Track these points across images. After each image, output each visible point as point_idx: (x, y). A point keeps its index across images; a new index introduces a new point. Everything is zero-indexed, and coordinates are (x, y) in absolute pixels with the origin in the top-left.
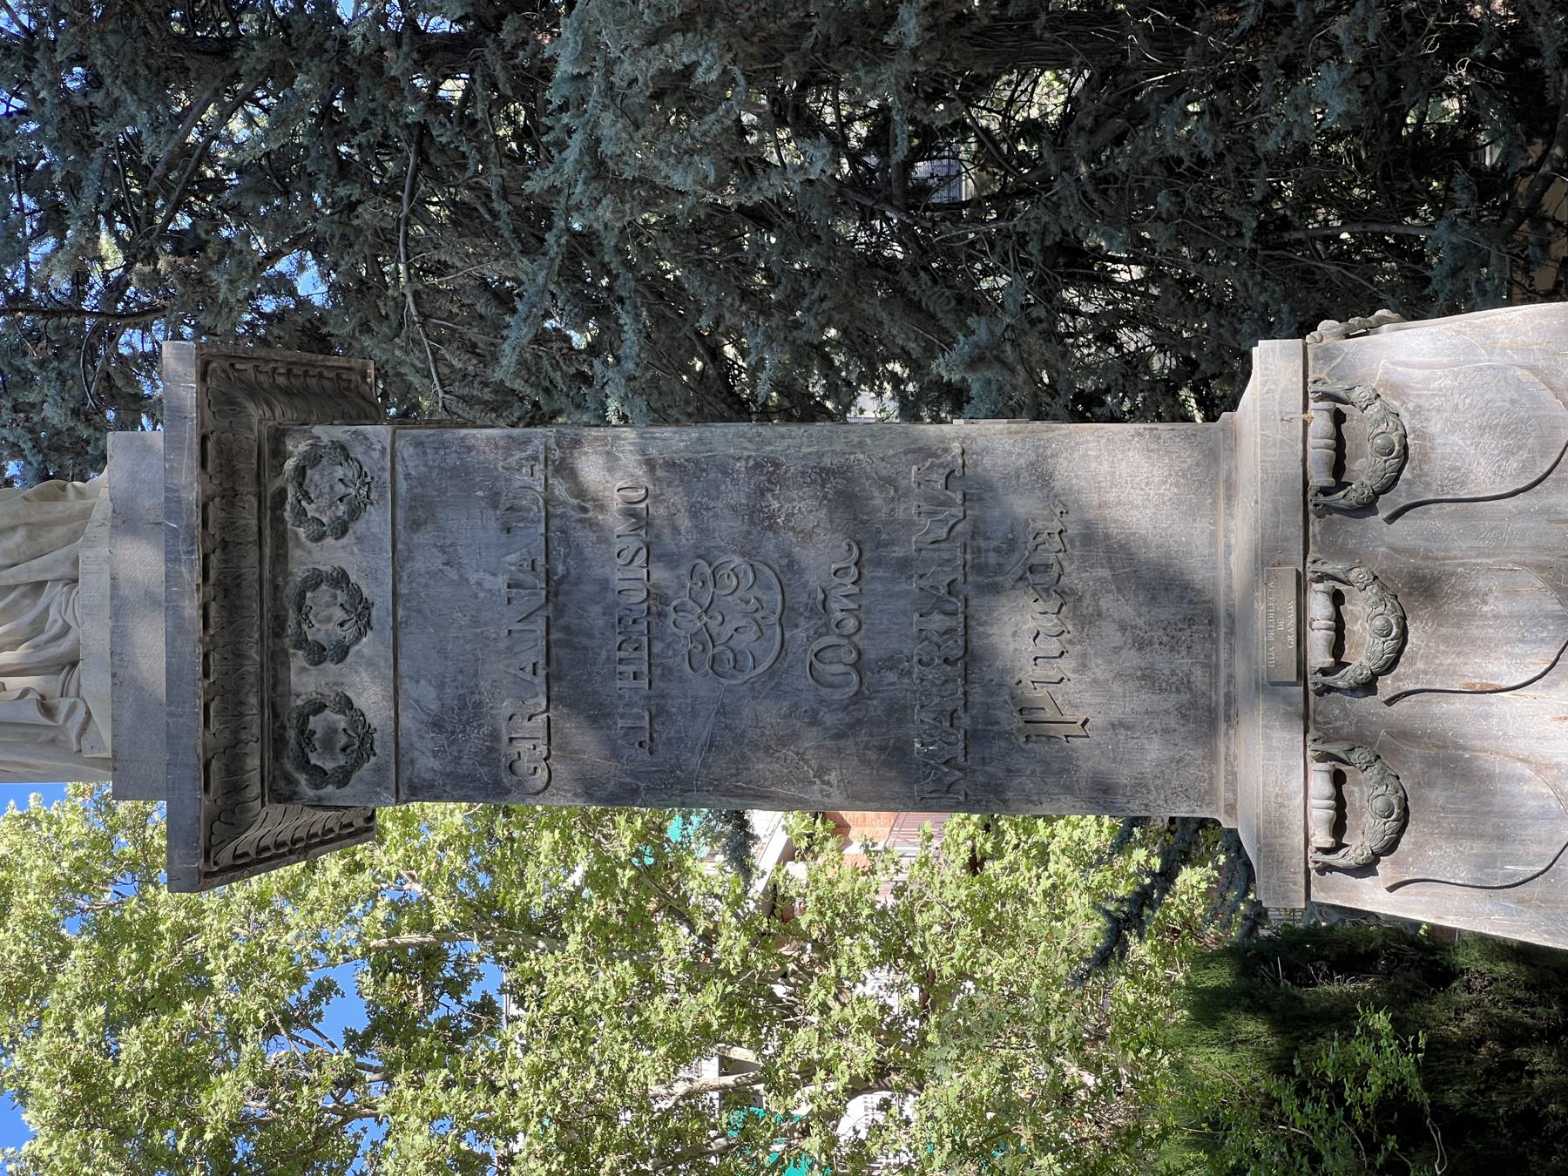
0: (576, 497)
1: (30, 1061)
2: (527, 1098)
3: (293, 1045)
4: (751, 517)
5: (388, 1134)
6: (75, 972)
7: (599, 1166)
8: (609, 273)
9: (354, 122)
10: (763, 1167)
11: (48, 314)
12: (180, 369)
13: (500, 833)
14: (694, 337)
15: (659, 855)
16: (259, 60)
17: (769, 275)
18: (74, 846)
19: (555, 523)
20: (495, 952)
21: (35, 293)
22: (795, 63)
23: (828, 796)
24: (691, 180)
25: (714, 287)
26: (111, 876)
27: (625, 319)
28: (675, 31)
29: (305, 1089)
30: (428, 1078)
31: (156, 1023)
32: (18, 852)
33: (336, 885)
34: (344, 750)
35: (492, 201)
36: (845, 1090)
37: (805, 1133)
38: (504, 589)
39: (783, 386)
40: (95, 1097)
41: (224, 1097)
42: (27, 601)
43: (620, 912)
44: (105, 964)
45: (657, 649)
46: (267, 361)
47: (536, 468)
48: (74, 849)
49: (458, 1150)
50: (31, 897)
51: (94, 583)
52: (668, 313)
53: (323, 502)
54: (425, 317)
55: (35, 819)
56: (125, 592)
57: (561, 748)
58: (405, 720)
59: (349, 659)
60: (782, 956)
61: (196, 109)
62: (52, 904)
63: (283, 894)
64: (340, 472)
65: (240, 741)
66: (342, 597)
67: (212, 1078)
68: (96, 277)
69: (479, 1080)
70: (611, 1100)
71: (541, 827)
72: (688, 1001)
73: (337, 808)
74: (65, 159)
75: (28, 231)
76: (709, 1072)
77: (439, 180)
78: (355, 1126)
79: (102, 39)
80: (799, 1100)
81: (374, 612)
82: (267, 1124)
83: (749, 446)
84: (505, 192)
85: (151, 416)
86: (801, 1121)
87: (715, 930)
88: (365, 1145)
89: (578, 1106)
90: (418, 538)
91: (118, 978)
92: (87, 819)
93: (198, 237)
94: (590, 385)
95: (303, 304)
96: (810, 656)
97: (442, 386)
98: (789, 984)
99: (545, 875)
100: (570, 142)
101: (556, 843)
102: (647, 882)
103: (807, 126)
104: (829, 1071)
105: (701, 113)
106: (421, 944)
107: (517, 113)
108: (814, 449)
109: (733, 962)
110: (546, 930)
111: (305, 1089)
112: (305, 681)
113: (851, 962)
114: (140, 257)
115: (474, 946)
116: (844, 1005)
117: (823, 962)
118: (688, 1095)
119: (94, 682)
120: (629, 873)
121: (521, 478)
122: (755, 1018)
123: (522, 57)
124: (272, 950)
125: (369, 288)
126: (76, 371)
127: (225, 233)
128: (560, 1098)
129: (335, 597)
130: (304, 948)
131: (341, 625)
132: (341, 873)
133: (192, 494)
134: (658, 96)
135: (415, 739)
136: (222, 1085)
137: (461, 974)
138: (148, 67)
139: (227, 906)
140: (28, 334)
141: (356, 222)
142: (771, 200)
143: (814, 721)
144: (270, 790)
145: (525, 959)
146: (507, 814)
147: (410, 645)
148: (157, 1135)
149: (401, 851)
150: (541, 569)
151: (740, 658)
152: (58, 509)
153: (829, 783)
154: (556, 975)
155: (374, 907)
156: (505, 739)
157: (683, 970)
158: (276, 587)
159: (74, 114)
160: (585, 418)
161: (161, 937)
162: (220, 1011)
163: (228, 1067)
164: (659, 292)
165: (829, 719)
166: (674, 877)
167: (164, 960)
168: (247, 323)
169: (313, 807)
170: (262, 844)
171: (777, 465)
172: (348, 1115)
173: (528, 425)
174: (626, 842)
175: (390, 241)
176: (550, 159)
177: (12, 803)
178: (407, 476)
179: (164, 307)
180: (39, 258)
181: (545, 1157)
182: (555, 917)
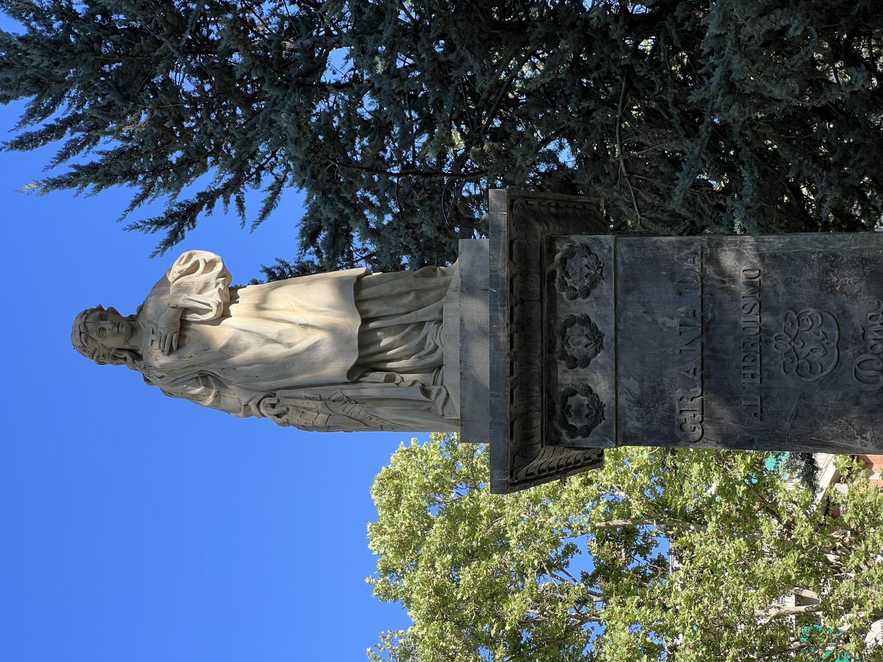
0: (719, 275)
1: (412, 583)
2: (684, 614)
3: (553, 580)
4: (820, 286)
5: (606, 631)
6: (436, 535)
7: (726, 655)
8: (735, 148)
9: (591, 66)
10: (821, 659)
11: (425, 175)
12: (498, 204)
13: (669, 464)
14: (784, 184)
15: (760, 478)
16: (540, 33)
17: (828, 146)
18: (435, 467)
19: (707, 289)
20: (666, 531)
21: (418, 164)
22: (847, 24)
23: (866, 446)
24: (785, 93)
25: (797, 154)
26: (455, 484)
27: (745, 174)
28: (776, 7)
29: (560, 604)
30: (628, 601)
31: (479, 565)
32: (405, 470)
33: (577, 492)
34: (587, 416)
35: (668, 107)
36: (870, 617)
37: (847, 640)
38: (678, 327)
39: (838, 211)
40: (447, 604)
41: (516, 607)
42: (415, 333)
43: (737, 510)
44: (452, 531)
45: (765, 361)
46: (545, 199)
47: (696, 259)
48: (435, 469)
49: (646, 642)
50: (412, 494)
51: (451, 323)
52: (770, 169)
53: (576, 278)
54: (630, 173)
55: (414, 452)
56: (468, 327)
57: (709, 416)
58: (622, 400)
59: (590, 366)
60: (832, 538)
61: (505, 61)
62: (423, 499)
63: (548, 496)
64: (586, 261)
65: (531, 411)
66: (586, 331)
67: (509, 596)
68: (450, 156)
69: (657, 603)
70: (733, 618)
71: (692, 461)
72: (778, 562)
73: (583, 449)
74: (434, 91)
75: (415, 130)
76: (789, 603)
77: (639, 97)
78: (587, 626)
79: (455, 25)
80: (843, 622)
81: (605, 339)
82: (539, 623)
83: (820, 245)
84: (676, 103)
85: (479, 231)
86: (844, 634)
87: (793, 522)
88: (593, 637)
89: (713, 620)
90: (630, 298)
91: (459, 540)
92: (441, 453)
93: (505, 131)
94: (724, 211)
95: (562, 167)
96: (855, 366)
97: (640, 213)
98: (837, 554)
99: (695, 488)
100: (714, 73)
101: (701, 470)
102: (754, 493)
103: (853, 61)
104: (861, 606)
105: (790, 54)
106: (624, 526)
107: (683, 57)
108: (858, 247)
109: (804, 541)
110: (695, 520)
111: (560, 604)
112: (566, 378)
113: (874, 543)
114: (474, 143)
115: (654, 527)
116: (870, 567)
117: (857, 542)
118: (777, 616)
119: (451, 377)
120: (743, 488)
121: (687, 265)
122: (817, 573)
123: (687, 26)
124: (542, 527)
125: (599, 158)
126: (439, 206)
127: (520, 129)
128: (703, 615)
129: (583, 331)
130: (559, 526)
131: (586, 346)
132: (580, 485)
133: (504, 274)
134: (766, 45)
135: (627, 411)
136: (515, 600)
137: (647, 543)
138: (480, 39)
139: (517, 502)
140: (414, 186)
141: (592, 121)
142: (832, 104)
143: (857, 403)
144: (546, 438)
145: (683, 536)
146: (673, 453)
147: (624, 357)
148: (480, 627)
149: (613, 473)
150: (699, 316)
151: (813, 366)
152: (432, 281)
153: (866, 439)
154: (701, 545)
155: (598, 504)
156: (678, 411)
157: (774, 544)
158: (550, 326)
159: (439, 66)
160: (721, 231)
161: (481, 518)
162: (513, 559)
163: (518, 590)
164: (764, 158)
165: (866, 401)
166: (769, 490)
167: (483, 531)
168: (531, 178)
169: (569, 448)
170: (542, 468)
171: (836, 256)
172: (584, 619)
173: (688, 235)
174: (742, 470)
175: (610, 131)
176: (702, 82)
177: (402, 443)
178: (623, 263)
179: (487, 170)
180: (420, 145)
181: (695, 648)
182: (700, 512)
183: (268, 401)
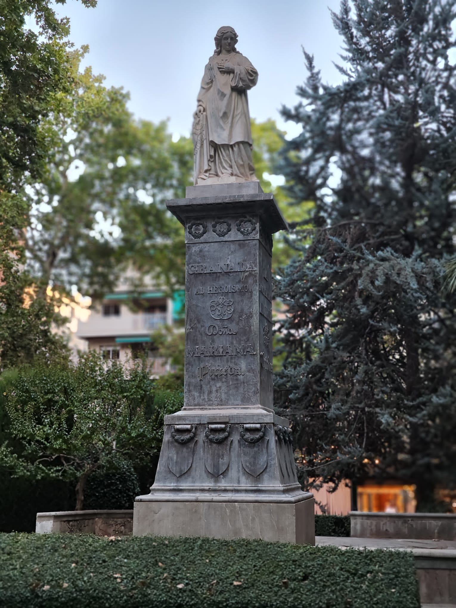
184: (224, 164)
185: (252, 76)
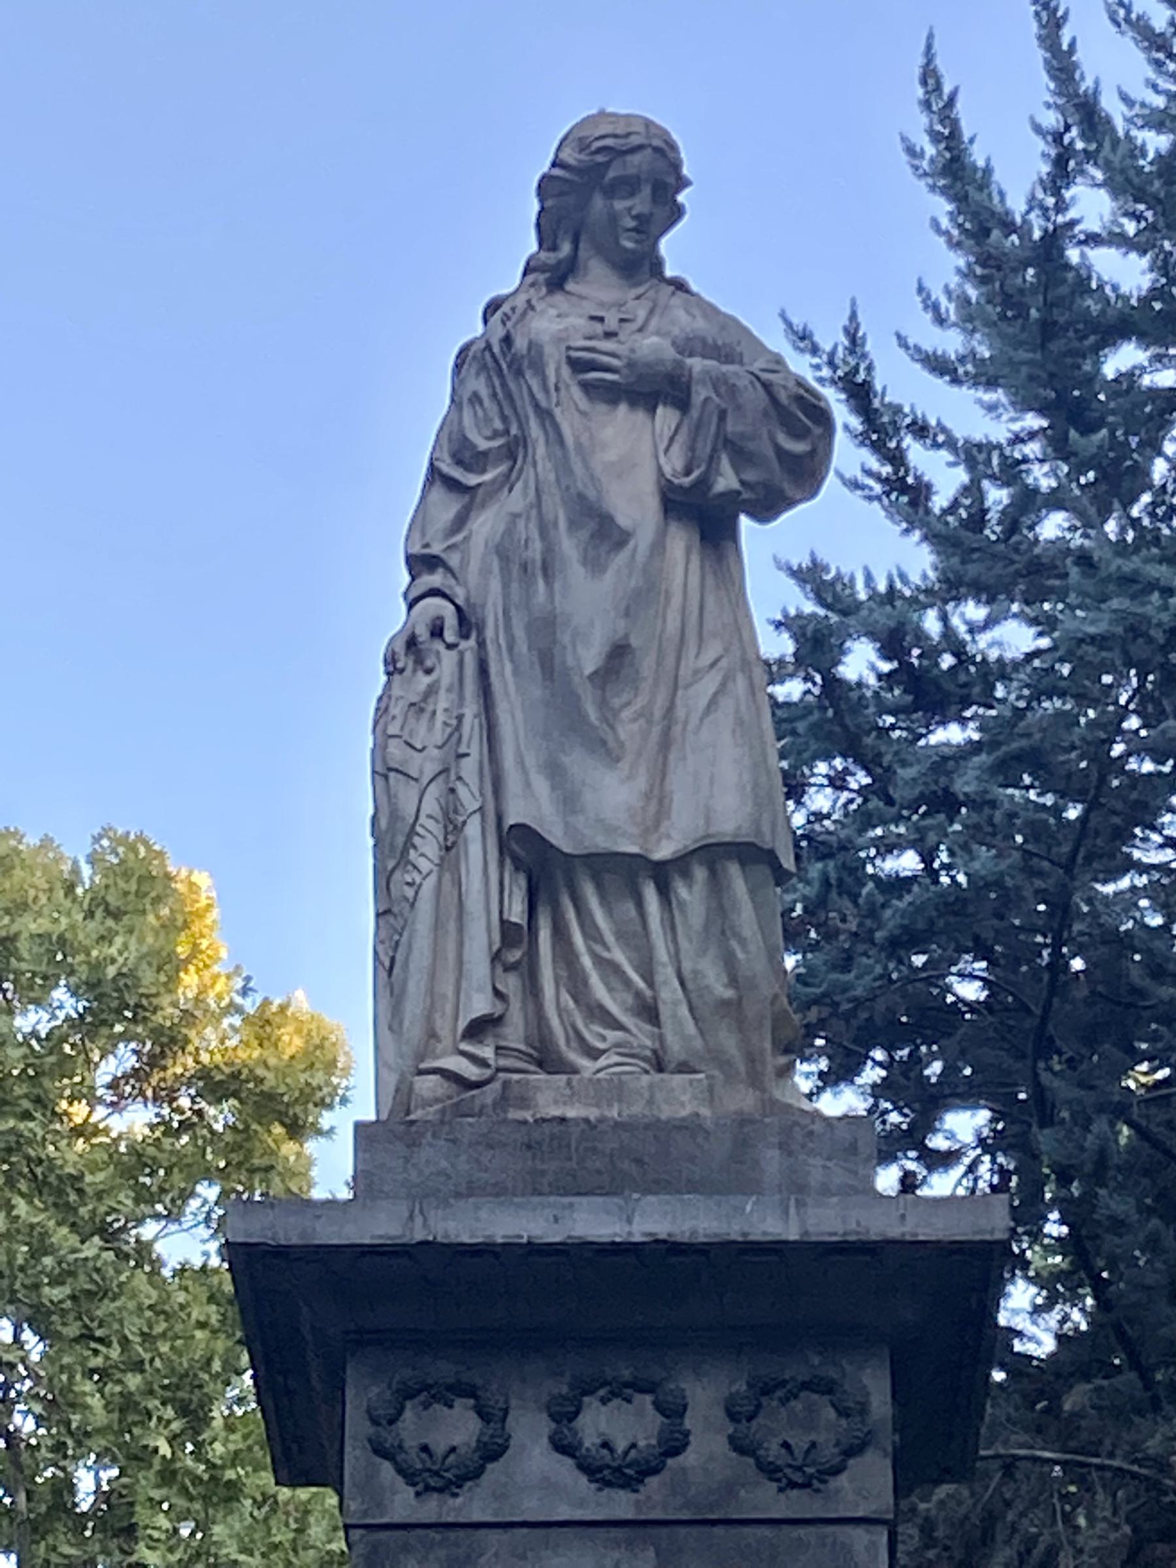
42: (630, 1000)
183: (451, 621)
184: (599, 990)
185: (798, 433)
